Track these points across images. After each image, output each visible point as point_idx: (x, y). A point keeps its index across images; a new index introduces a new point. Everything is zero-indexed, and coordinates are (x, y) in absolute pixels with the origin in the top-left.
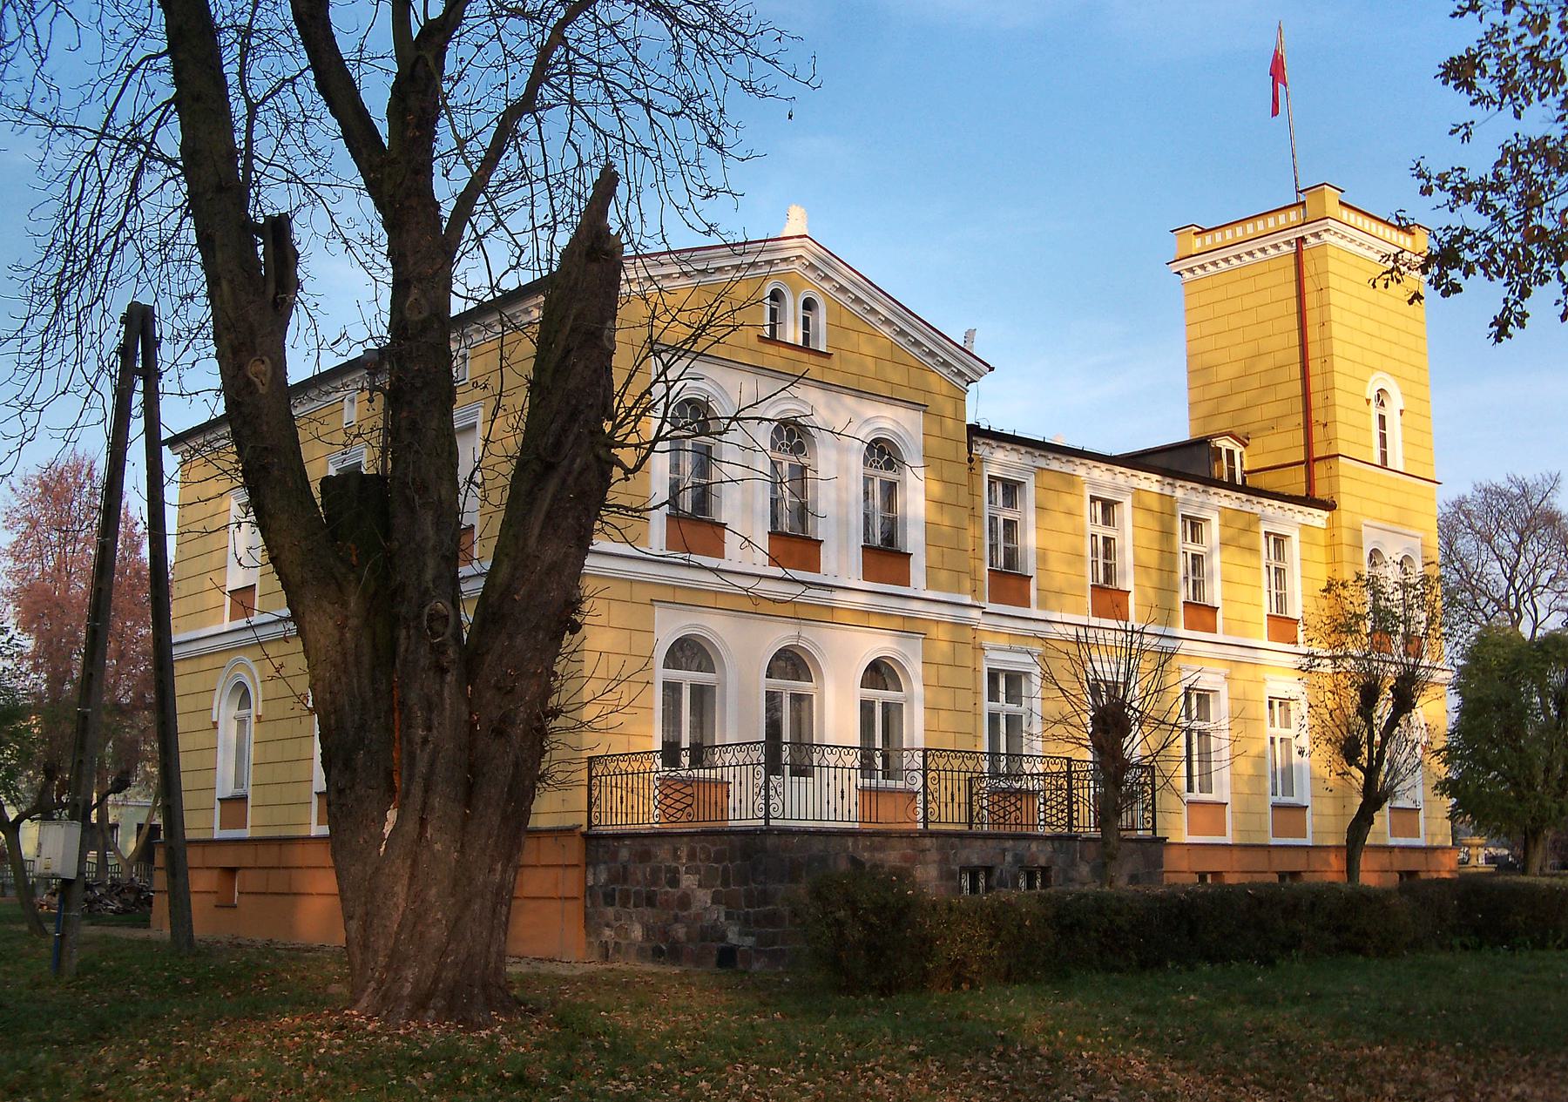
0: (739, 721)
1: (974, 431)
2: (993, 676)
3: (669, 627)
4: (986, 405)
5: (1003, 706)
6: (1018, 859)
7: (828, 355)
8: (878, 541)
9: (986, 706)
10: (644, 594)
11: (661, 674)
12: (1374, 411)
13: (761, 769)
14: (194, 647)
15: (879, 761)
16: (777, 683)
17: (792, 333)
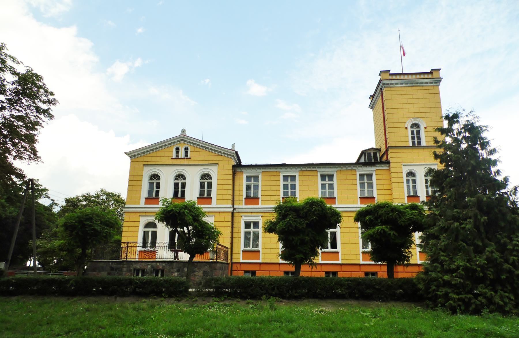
6: (152, 267)
7: (190, 158)
10: (138, 214)
17: (182, 154)
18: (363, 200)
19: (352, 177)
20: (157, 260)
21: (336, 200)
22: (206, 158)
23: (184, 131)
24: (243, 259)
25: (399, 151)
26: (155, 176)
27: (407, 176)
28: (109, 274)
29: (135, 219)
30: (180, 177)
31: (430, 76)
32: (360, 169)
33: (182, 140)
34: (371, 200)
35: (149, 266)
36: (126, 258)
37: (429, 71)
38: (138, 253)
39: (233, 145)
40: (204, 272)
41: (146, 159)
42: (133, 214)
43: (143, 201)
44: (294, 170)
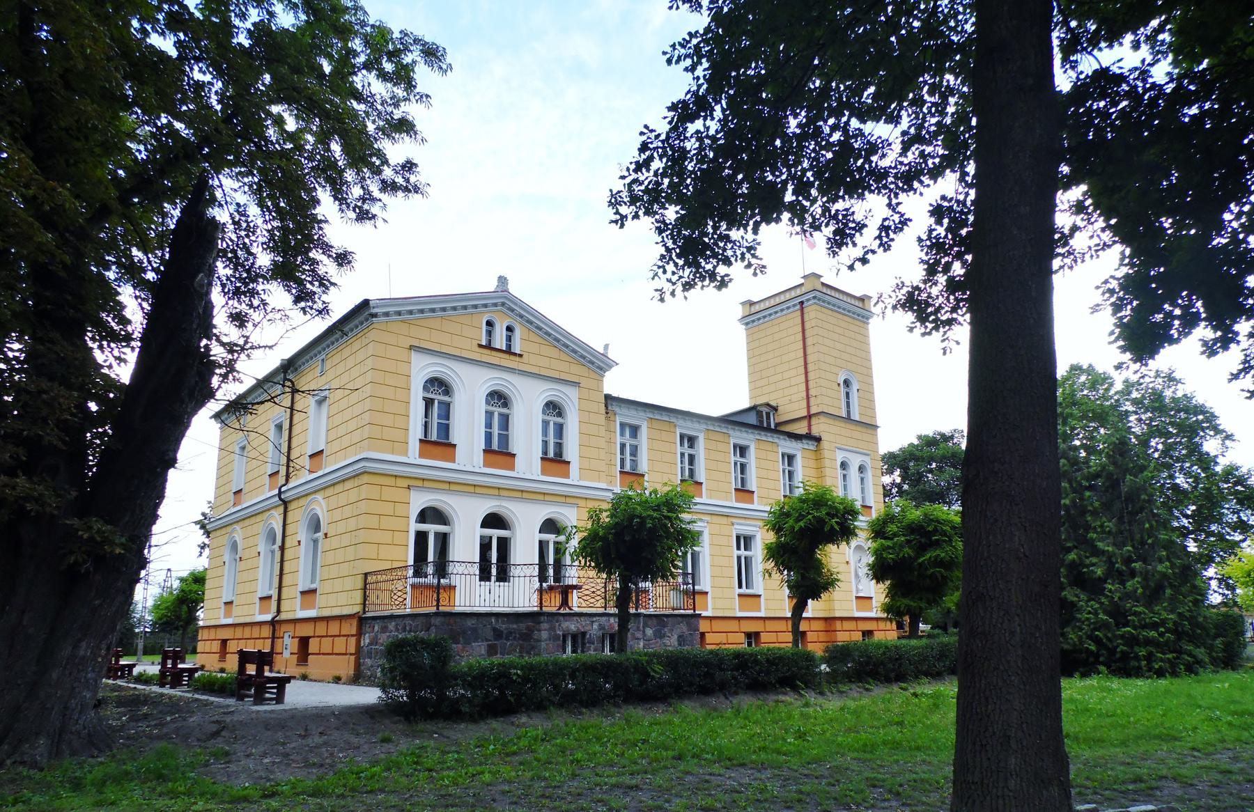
0: (465, 547)
1: (608, 398)
2: (738, 538)
3: (419, 501)
4: (614, 384)
5: (743, 552)
6: (601, 627)
7: (521, 356)
8: (551, 455)
9: (736, 553)
10: (405, 483)
11: (414, 527)
12: (842, 389)
13: (537, 579)
14: (356, 467)
15: (551, 572)
16: (546, 537)
17: (500, 341)
18: (429, 447)
19: (721, 446)
20: (457, 609)
21: (755, 495)
22: (556, 364)
23: (502, 280)
24: (740, 610)
25: (831, 421)
26: (438, 384)
27: (425, 388)
28: (492, 650)
29: (398, 494)
30: (438, 384)
31: (857, 303)
32: (738, 433)
33: (503, 304)
34: (746, 495)
35: (595, 626)
36: (438, 606)
37: (858, 295)
38: (409, 589)
39: (606, 347)
40: (680, 637)
41: (415, 331)
42: (391, 481)
43: (414, 446)
44: (696, 426)
